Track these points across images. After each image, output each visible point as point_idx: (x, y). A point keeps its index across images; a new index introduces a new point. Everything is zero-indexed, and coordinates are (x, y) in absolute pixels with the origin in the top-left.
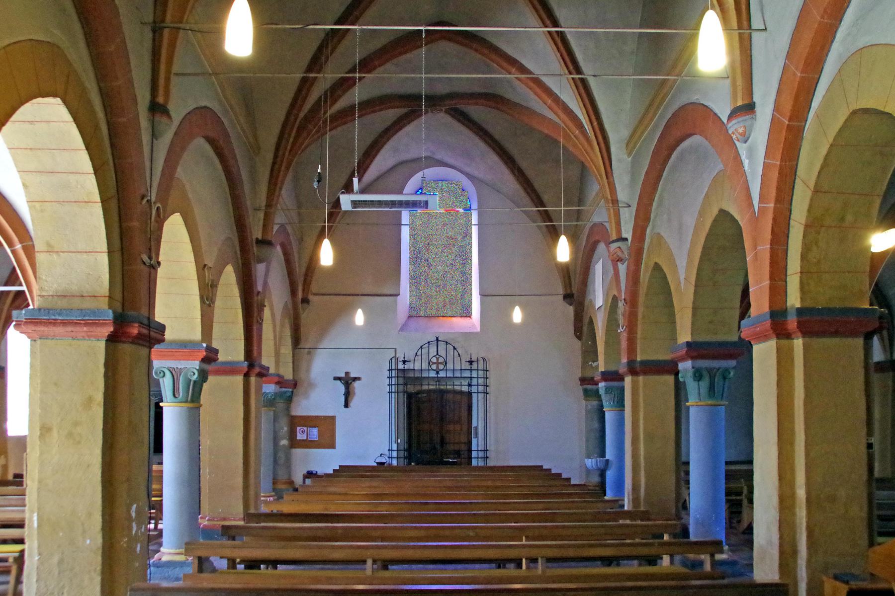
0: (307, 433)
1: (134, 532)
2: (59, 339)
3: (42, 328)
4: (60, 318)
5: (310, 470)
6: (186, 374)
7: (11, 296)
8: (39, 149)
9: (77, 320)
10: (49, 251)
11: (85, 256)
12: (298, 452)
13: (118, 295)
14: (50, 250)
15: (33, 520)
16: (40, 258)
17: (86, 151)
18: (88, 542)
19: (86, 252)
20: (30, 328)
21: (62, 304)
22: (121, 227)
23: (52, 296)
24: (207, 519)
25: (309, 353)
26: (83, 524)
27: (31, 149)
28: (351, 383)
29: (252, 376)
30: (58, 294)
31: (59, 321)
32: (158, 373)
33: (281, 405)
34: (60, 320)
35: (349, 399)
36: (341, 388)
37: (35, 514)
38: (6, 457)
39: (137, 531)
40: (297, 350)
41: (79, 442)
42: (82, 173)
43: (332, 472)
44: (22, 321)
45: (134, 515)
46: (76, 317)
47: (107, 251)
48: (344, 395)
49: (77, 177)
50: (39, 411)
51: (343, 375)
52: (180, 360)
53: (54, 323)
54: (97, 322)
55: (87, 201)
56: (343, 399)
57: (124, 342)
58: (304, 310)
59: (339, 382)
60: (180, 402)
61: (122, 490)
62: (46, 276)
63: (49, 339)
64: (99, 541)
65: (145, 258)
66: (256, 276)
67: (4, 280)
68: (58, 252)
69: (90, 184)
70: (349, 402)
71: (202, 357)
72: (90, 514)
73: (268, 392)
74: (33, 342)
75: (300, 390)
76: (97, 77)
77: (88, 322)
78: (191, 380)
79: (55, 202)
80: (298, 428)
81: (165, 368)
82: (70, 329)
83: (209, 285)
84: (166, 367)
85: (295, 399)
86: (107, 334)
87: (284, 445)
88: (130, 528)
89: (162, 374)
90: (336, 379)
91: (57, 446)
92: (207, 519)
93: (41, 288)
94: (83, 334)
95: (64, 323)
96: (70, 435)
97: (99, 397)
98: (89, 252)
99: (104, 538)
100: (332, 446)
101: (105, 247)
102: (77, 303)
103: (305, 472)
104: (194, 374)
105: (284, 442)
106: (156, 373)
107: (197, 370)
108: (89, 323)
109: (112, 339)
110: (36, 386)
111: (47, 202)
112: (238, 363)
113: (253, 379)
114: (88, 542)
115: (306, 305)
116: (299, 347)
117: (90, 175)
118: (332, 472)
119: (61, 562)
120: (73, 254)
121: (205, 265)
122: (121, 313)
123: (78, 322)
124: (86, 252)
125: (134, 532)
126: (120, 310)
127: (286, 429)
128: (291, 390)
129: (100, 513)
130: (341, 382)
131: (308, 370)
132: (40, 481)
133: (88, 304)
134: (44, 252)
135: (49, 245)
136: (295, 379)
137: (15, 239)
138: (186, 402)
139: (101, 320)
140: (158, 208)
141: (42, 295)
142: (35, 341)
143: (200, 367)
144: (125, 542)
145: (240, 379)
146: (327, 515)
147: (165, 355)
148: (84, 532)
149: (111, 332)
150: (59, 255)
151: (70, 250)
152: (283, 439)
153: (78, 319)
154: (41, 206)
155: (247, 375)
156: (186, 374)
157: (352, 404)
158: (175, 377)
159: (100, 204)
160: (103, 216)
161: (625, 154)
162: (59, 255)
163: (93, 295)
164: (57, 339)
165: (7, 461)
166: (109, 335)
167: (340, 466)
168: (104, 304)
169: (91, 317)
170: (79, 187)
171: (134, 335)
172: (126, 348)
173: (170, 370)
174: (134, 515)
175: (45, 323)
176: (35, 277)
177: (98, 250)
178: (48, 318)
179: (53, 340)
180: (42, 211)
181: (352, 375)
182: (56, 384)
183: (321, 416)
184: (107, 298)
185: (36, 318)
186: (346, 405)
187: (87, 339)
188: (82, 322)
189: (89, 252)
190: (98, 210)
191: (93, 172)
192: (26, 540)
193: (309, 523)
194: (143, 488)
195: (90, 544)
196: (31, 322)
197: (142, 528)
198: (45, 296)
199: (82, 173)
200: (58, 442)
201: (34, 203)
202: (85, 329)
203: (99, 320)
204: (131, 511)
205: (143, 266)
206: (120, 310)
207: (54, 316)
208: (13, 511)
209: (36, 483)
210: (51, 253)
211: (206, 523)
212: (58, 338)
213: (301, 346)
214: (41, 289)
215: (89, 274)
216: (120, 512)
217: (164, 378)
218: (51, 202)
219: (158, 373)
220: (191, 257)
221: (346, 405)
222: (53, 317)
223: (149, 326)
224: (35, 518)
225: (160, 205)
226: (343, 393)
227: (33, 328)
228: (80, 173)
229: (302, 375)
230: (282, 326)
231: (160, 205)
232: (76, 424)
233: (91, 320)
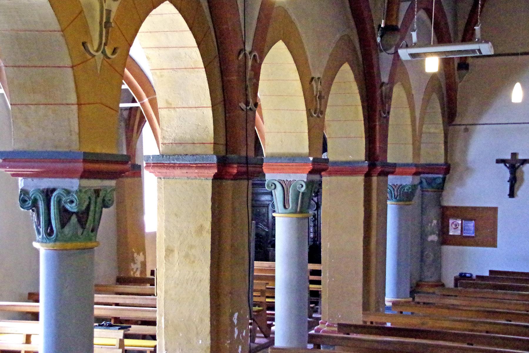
0: (462, 228)
1: (236, 336)
3: (164, 170)
4: (178, 162)
5: (464, 272)
6: (295, 186)
8: (157, 32)
9: (190, 164)
10: (168, 107)
11: (194, 110)
12: (449, 250)
13: (222, 141)
14: (169, 107)
15: (161, 321)
16: (161, 112)
17: (190, 32)
18: (200, 342)
19: (196, 107)
20: (157, 170)
21: (180, 150)
22: (223, 81)
23: (172, 143)
24: (326, 324)
25: (466, 130)
26: (197, 328)
27: (150, 32)
28: (519, 166)
29: (374, 176)
30: (176, 142)
31: (177, 165)
33: (430, 194)
34: (178, 164)
35: (516, 185)
36: (507, 174)
37: (163, 318)
38: (144, 254)
39: (238, 335)
40: (451, 128)
41: (194, 262)
42: (189, 47)
43: (487, 274)
44: (150, 164)
45: (235, 321)
46: (190, 161)
47: (211, 106)
48: (508, 181)
49: (186, 50)
50: (165, 236)
51: (509, 157)
52: (290, 173)
53: (174, 166)
54: (205, 165)
55: (194, 67)
56: (507, 186)
57: (226, 179)
58: (461, 77)
59: (502, 165)
60: (290, 213)
61: (226, 300)
62: (167, 127)
63: (170, 178)
64: (209, 341)
65: (243, 106)
66: (378, 69)
68: (175, 108)
69: (195, 55)
70: (515, 191)
71: (310, 170)
72: (202, 320)
73: (405, 184)
74: (159, 180)
75: (454, 174)
77: (199, 165)
78: (300, 192)
79: (170, 69)
80: (451, 221)
81: (276, 180)
82: (185, 171)
83: (317, 97)
84: (277, 179)
85: (447, 186)
86: (213, 175)
87: (432, 241)
88: (233, 332)
89: (273, 186)
90: (499, 161)
91: (178, 264)
92: (326, 324)
93: (164, 137)
94: (196, 175)
95: (181, 166)
96: (187, 256)
97: (208, 226)
98: (198, 107)
99: (212, 339)
100: (494, 244)
101: (209, 103)
102: (190, 149)
103: (457, 274)
104: (302, 186)
105: (433, 238)
106: (268, 186)
107: (304, 182)
108: (198, 166)
109: (216, 178)
110: (162, 215)
111: (165, 69)
112: (358, 162)
113: (375, 179)
114: (200, 342)
115: (464, 72)
116: (454, 123)
117: (195, 48)
118: (487, 274)
120: (186, 109)
121: (313, 78)
122: (224, 157)
123: (192, 165)
124: (196, 107)
125: (236, 336)
126: (223, 153)
127: (435, 222)
128: (441, 176)
129: (209, 319)
130: (506, 165)
131: (465, 152)
132: (166, 292)
133: (199, 150)
134: (165, 108)
135: (167, 102)
136: (449, 162)
137: (143, 94)
138: (295, 212)
139: (208, 163)
140: (255, 56)
141: (164, 142)
142: (160, 178)
143: (307, 179)
144: (228, 343)
145: (360, 179)
146: (423, 331)
147: (274, 169)
148: (197, 333)
149: (216, 173)
150: (176, 111)
151: (184, 106)
152: (432, 233)
153: (191, 163)
155: (368, 176)
156: (295, 186)
157: (520, 192)
158: (285, 190)
159: (204, 69)
160: (206, 79)
162: (176, 111)
163: (201, 142)
164: (176, 179)
165: (145, 258)
166: (214, 175)
167: (491, 272)
168: (210, 149)
169: (200, 161)
170: (187, 57)
171: (234, 174)
172: (228, 184)
173: (280, 183)
174: (235, 321)
175: (167, 166)
176: (159, 125)
177: (205, 106)
178: (169, 162)
179: (173, 180)
181: (520, 157)
182: (176, 215)
183: (479, 208)
184: (213, 145)
185: (161, 162)
186: (512, 194)
187: (198, 178)
188: (194, 165)
189: (198, 107)
190: (202, 74)
191: (197, 46)
192: (157, 338)
193: (395, 336)
194: (245, 298)
195: (202, 344)
196: (157, 166)
197: (243, 332)
198: (167, 143)
199: (189, 47)
200: (178, 262)
201: (155, 71)
202: (196, 171)
203: (206, 164)
204: (234, 319)
205: (241, 112)
206: (223, 153)
207: (173, 160)
208: (149, 311)
209: (163, 293)
210: (170, 109)
211: (326, 329)
213: (458, 120)
214: (164, 138)
215: (198, 125)
216: (225, 319)
217: (276, 190)
218: (168, 69)
219: (270, 185)
220: (295, 75)
221: (512, 194)
222: (173, 162)
223: (247, 163)
224: (163, 321)
225: (257, 54)
226: (508, 179)
227: (159, 170)
228: (187, 47)
229: (457, 157)
230: (426, 101)
231: (257, 54)
232: (191, 247)
233: (200, 164)
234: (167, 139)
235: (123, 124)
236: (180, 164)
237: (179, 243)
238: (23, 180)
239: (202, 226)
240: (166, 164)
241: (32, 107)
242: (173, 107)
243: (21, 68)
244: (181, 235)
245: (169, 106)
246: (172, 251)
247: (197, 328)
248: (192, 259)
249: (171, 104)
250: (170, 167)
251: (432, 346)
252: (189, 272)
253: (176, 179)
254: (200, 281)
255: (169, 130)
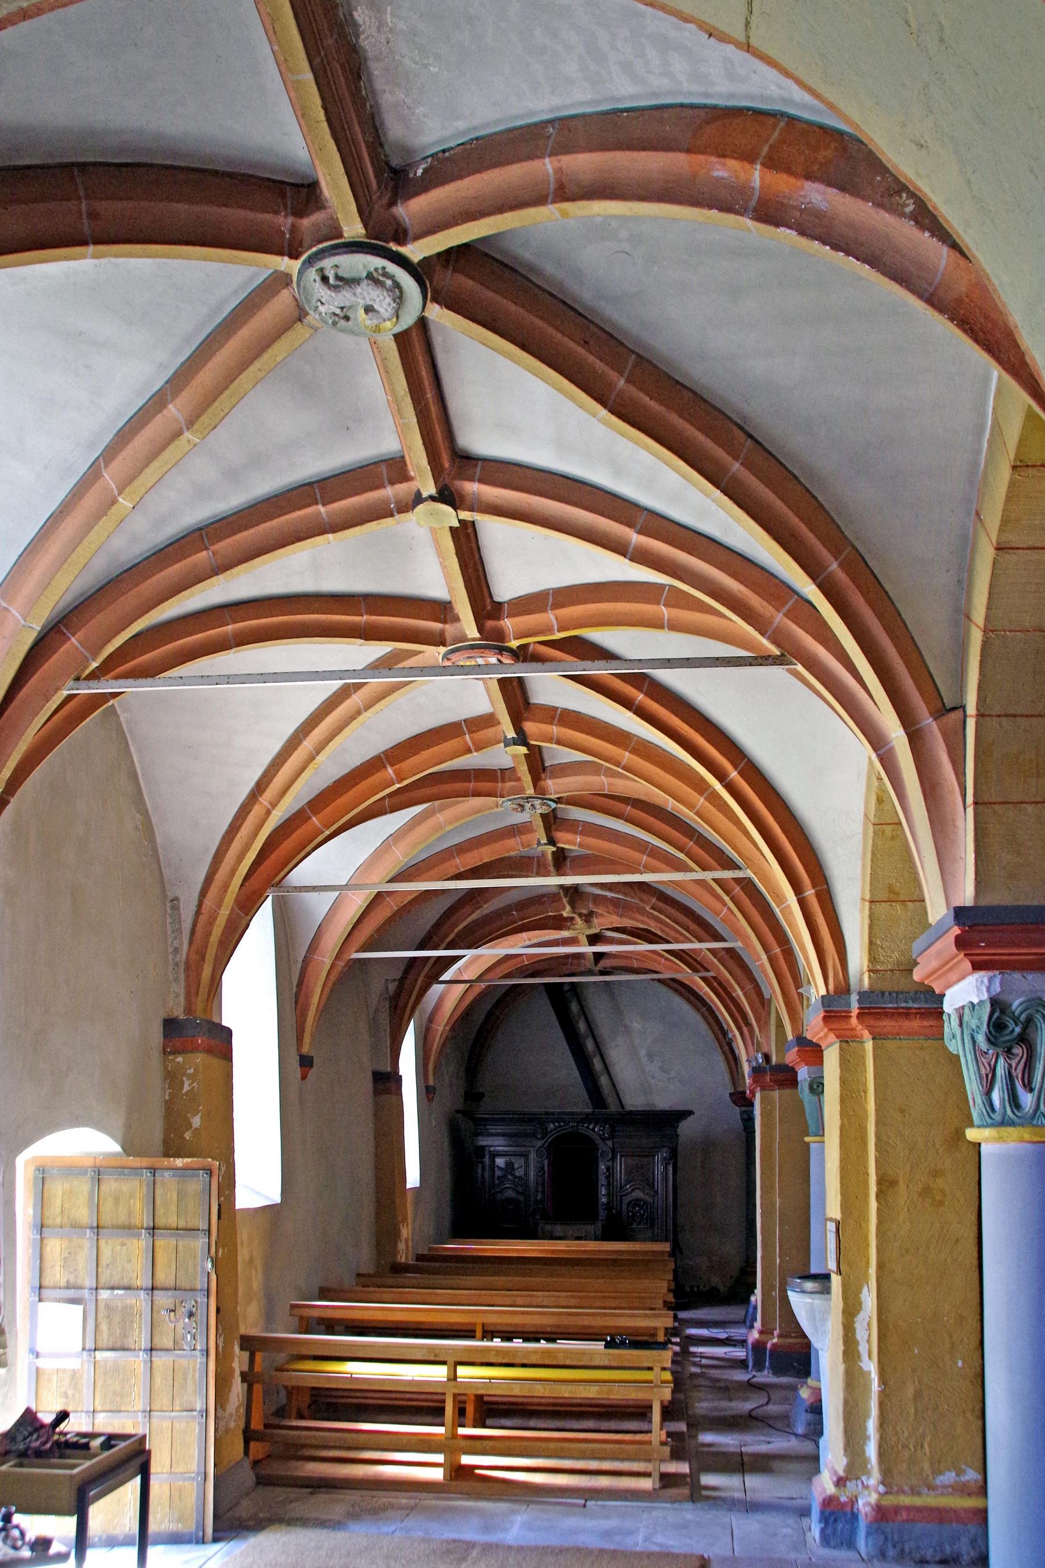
2: (905, 1039)
4: (915, 1006)
7: (430, 964)
18: (960, 1363)
23: (892, 971)
26: (951, 1336)
30: (901, 968)
31: (914, 1011)
32: (815, 1087)
34: (915, 1008)
41: (941, 1203)
67: (418, 940)
76: (259, 503)
91: (906, 1210)
96: (926, 1191)
114: (960, 1363)
119: (918, 1395)
154: (893, 830)
161: (877, 213)
164: (900, 1039)
178: (896, 1006)
180: (893, 838)
195: (963, 1367)
196: (870, 1014)
207: (906, 1002)
212: (902, 1037)
219: (815, 1087)
222: (903, 1005)
232: (936, 1174)
234: (883, 963)
235: (387, 1004)
236: (919, 1009)
237: (908, 1168)
238: (999, 977)
239: (957, 1132)
240: (890, 1008)
241: (1030, 808)
242: (902, 898)
243: (1019, 719)
244: (911, 1150)
245: (893, 897)
246: (893, 1183)
247: (951, 1336)
248: (938, 1198)
249: (897, 894)
250: (899, 1014)
251: (722, 1384)
252: (932, 1224)
253: (900, 1039)
254: (957, 1240)
255: (887, 944)
